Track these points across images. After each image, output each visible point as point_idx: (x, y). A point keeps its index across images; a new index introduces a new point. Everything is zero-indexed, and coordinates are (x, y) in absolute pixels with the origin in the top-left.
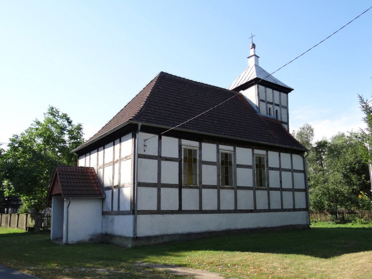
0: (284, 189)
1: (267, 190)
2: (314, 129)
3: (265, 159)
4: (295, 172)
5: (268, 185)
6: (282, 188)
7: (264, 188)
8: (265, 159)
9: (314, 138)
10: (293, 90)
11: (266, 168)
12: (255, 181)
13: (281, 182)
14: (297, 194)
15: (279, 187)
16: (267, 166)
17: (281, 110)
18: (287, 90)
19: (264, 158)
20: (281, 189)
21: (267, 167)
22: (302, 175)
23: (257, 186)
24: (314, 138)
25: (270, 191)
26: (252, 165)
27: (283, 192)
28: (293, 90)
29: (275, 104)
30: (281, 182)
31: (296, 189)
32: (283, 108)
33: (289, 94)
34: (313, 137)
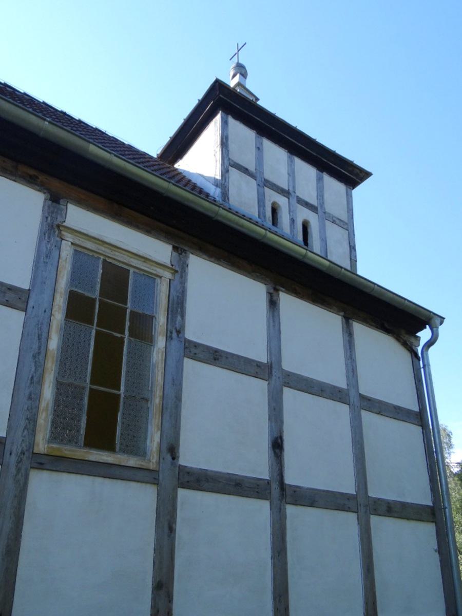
0: (296, 489)
1: (155, 481)
2: (453, 433)
3: (162, 290)
4: (369, 410)
5: (173, 451)
6: (282, 485)
7: (132, 461)
8: (162, 290)
9: (454, 453)
10: (367, 175)
11: (161, 342)
12: (35, 397)
13: (277, 445)
14: (382, 526)
15: (266, 476)
16: (176, 331)
17: (323, 229)
18: (350, 175)
19: (152, 278)
20: (275, 489)
21: (169, 338)
22: (427, 531)
23: (56, 436)
24: (454, 453)
25: (181, 492)
26: (26, 286)
27: (290, 510)
28: (367, 175)
29: (298, 197)
30: (277, 445)
31: (377, 501)
32: (334, 222)
33: (357, 192)
34: (451, 450)
